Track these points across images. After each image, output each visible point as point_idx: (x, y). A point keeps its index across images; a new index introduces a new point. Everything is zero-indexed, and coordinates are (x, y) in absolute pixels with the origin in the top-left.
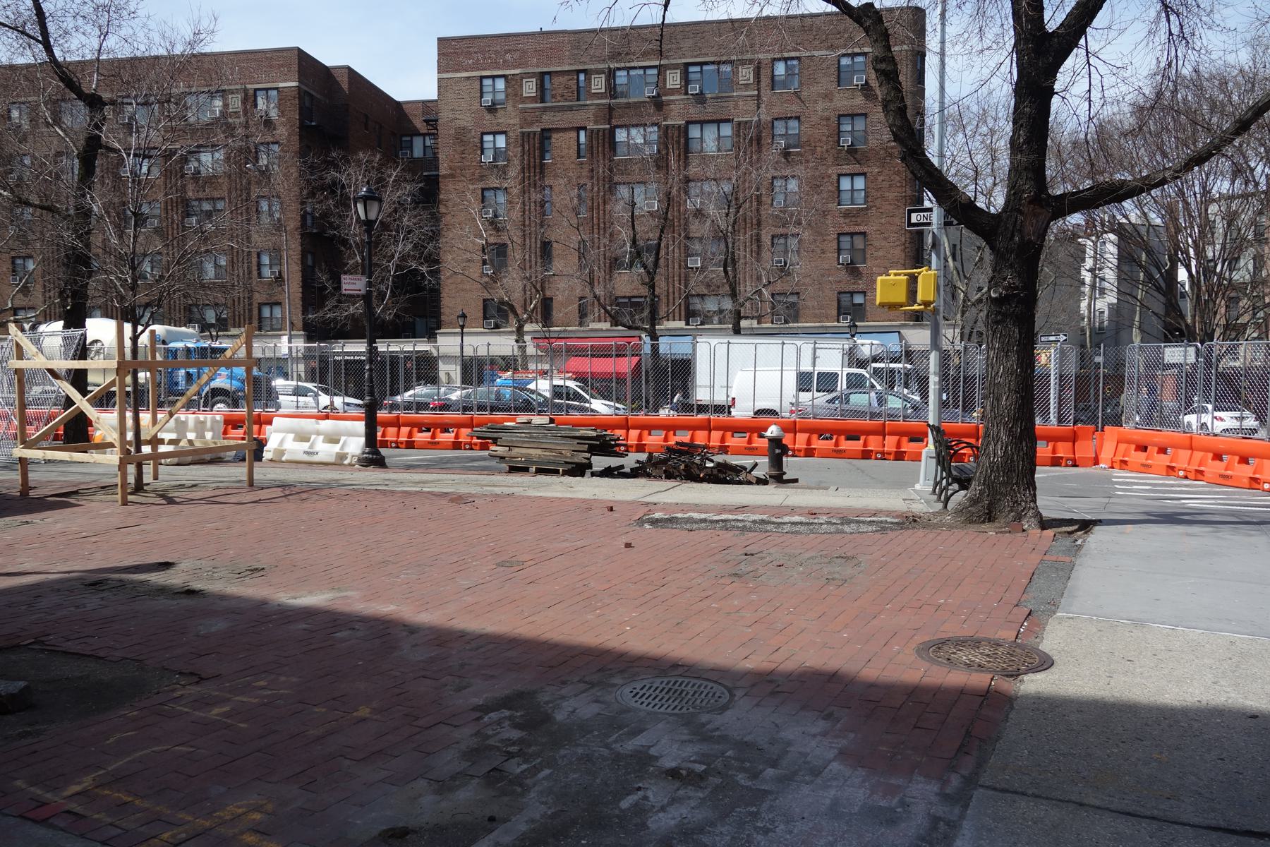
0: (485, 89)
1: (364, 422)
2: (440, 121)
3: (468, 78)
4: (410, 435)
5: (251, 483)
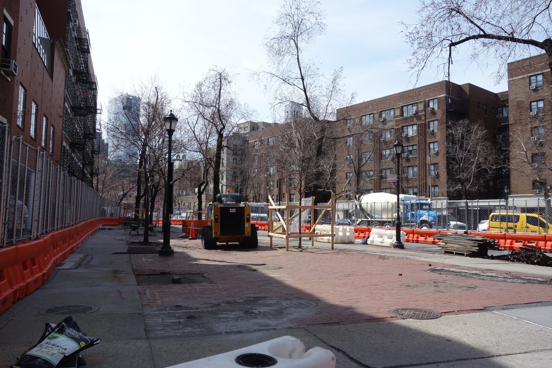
0: (532, 82)
1: (395, 231)
2: (509, 100)
3: (523, 78)
4: (418, 238)
5: (333, 248)
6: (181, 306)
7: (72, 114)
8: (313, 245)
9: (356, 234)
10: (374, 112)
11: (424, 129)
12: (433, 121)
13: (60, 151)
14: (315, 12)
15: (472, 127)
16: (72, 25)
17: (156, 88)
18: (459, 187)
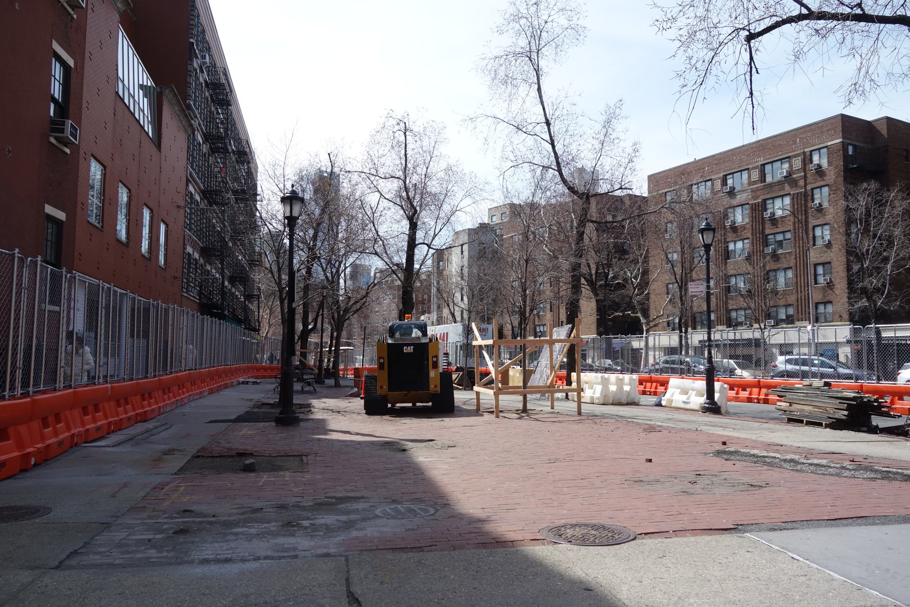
1: (705, 382)
5: (580, 413)
6: (192, 511)
7: (204, 203)
8: (552, 408)
9: (732, 393)
10: (713, 177)
11: (803, 202)
12: (821, 187)
13: (182, 262)
14: (568, 8)
15: (885, 195)
16: (197, 63)
17: (329, 154)
18: (864, 303)
